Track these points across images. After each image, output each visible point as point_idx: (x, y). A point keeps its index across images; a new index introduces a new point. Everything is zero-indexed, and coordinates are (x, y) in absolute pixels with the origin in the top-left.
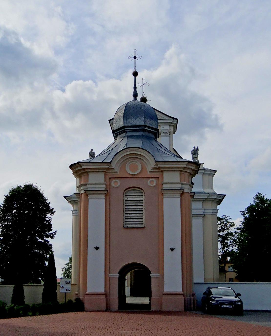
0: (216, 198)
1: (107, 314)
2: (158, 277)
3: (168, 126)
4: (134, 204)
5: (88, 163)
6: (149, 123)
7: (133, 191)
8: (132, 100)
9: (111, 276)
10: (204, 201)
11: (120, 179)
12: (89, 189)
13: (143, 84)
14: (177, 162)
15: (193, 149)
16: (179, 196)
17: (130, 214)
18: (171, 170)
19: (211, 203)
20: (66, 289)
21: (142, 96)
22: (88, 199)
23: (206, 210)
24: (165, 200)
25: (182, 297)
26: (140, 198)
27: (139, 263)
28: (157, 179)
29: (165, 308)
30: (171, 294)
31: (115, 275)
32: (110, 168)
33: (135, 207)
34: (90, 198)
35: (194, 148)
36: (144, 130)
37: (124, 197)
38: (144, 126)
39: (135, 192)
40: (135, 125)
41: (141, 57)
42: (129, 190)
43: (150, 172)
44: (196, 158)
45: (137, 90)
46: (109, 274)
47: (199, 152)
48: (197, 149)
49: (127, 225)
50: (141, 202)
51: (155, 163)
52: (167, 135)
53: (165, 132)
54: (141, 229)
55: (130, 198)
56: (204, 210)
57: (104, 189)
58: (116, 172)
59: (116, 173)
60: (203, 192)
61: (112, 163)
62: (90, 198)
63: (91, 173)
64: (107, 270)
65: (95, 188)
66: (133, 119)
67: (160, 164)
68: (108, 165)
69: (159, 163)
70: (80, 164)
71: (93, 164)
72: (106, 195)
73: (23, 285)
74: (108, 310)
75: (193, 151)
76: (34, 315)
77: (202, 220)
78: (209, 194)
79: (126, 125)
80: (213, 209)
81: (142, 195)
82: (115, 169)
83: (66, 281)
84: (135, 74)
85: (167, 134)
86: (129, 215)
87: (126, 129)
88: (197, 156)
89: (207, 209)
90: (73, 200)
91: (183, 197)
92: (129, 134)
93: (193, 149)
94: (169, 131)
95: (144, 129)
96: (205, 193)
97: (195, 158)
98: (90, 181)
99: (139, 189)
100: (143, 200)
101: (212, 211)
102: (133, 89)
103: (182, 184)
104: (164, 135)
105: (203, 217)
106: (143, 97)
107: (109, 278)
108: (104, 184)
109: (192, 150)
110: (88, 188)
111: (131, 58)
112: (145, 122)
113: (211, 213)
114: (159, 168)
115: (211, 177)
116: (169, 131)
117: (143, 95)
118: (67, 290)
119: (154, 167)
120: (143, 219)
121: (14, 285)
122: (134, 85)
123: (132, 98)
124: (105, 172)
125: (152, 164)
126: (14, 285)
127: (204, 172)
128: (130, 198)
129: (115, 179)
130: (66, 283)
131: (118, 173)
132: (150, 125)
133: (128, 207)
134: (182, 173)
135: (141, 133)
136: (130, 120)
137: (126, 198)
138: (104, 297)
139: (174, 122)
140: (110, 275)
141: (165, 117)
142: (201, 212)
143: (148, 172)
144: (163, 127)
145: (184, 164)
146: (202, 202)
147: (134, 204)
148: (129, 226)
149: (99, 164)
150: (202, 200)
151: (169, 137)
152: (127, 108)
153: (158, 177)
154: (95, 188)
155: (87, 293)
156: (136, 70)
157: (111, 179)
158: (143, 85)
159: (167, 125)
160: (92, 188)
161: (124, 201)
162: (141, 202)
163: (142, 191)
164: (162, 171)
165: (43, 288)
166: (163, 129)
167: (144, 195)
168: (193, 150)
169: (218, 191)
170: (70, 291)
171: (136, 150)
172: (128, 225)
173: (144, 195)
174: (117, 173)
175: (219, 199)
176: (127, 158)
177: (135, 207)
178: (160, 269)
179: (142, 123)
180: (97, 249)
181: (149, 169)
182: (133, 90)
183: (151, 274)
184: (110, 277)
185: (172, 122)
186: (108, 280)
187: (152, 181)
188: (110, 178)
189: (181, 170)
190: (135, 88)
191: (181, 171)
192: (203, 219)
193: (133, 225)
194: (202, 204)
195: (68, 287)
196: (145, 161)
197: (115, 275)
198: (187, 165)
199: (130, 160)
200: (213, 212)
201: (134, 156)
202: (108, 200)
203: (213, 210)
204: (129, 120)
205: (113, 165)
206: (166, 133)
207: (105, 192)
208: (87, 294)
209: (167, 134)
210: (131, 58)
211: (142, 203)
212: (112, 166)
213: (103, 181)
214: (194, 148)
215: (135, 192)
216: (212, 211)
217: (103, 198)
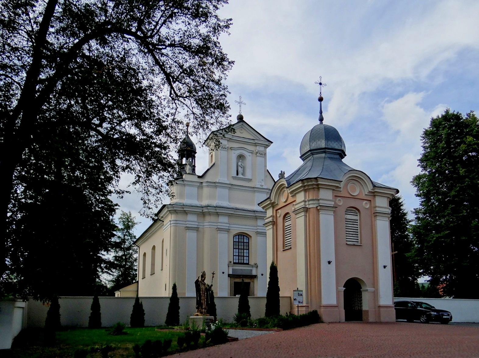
15: (280, 173)
21: (239, 114)
29: (383, 320)
30: (385, 307)
33: (352, 226)
35: (282, 171)
39: (352, 212)
43: (366, 195)
45: (323, 114)
51: (372, 187)
57: (332, 206)
63: (322, 189)
65: (327, 204)
73: (99, 297)
79: (327, 147)
81: (357, 215)
87: (327, 150)
90: (175, 209)
93: (280, 173)
98: (320, 197)
99: (355, 210)
104: (260, 155)
108: (332, 201)
111: (317, 83)
118: (299, 302)
119: (371, 191)
120: (358, 237)
121: (93, 297)
122: (319, 110)
123: (319, 123)
126: (93, 297)
135: (323, 155)
143: (364, 194)
151: (264, 158)
153: (370, 201)
154: (327, 204)
162: (357, 221)
163: (357, 212)
166: (259, 149)
167: (358, 216)
173: (358, 216)
177: (352, 226)
182: (319, 114)
187: (339, 200)
189: (389, 196)
193: (354, 243)
202: (182, 212)
210: (317, 83)
211: (357, 222)
215: (352, 212)
217: (332, 215)
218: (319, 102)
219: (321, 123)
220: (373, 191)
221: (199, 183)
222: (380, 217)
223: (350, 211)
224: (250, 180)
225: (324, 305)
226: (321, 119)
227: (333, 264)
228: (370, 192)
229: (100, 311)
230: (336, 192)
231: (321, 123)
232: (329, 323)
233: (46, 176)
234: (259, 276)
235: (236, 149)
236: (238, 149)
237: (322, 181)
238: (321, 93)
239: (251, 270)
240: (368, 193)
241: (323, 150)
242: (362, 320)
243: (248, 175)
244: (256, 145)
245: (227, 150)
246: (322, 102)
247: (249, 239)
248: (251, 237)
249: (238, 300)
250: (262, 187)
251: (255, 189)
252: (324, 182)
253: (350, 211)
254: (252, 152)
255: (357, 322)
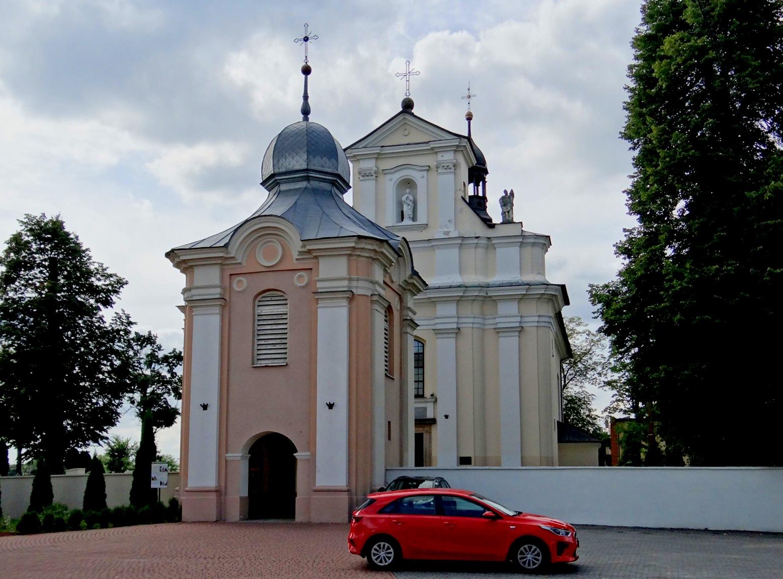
0: (543, 292)
1: (218, 529)
2: (307, 458)
3: (452, 153)
4: (272, 322)
5: (188, 250)
6: (319, 163)
7: (271, 298)
8: (296, 122)
9: (229, 457)
10: (522, 299)
11: (245, 276)
12: (194, 298)
13: (408, 73)
14: (337, 239)
15: (504, 195)
16: (345, 303)
17: (266, 341)
18: (332, 253)
19: (537, 302)
20: (161, 482)
21: (406, 97)
22: (193, 316)
23: (460, 324)
24: (320, 312)
25: (345, 496)
26: (282, 310)
27: (277, 433)
28: (310, 271)
30: (329, 491)
31: (235, 455)
32: (226, 256)
33: (274, 327)
34: (195, 313)
35: (505, 192)
36: (308, 179)
37: (256, 308)
38: (307, 170)
39: (274, 298)
40: (292, 169)
41: (296, 41)
42: (264, 295)
43: (297, 259)
44: (508, 212)
46: (226, 453)
47: (515, 201)
48: (510, 193)
49: (259, 362)
50: (284, 317)
52: (449, 170)
53: (446, 165)
54: (281, 368)
55: (266, 310)
56: (521, 317)
57: (218, 296)
58: (240, 263)
59: (239, 266)
60: (520, 282)
61: (230, 247)
62: (195, 315)
64: (223, 445)
65: (207, 295)
66: (289, 159)
67: (310, 245)
68: (222, 252)
69: (309, 242)
70: (175, 252)
71: (199, 251)
72: (223, 307)
74: (221, 520)
75: (503, 198)
76: (90, 527)
77: (454, 339)
78: (528, 284)
79: (277, 171)
80: (538, 314)
82: (237, 257)
83: (161, 467)
84: (307, 71)
85: (450, 168)
86: (263, 342)
88: (509, 209)
89: (526, 315)
91: (354, 304)
92: (283, 187)
93: (504, 195)
94: (452, 163)
95: (308, 176)
96: (518, 284)
97: (507, 213)
100: (287, 314)
101: (536, 319)
102: (302, 99)
103: (350, 280)
105: (457, 333)
106: (407, 98)
107: (226, 461)
109: (500, 197)
110: (193, 296)
111: (299, 40)
112: (308, 161)
113: (536, 324)
114: (309, 251)
115: (538, 250)
116: (452, 163)
117: (408, 94)
118: (161, 483)
119: (301, 250)
122: (303, 92)
124: (221, 264)
125: (296, 246)
127: (521, 240)
128: (266, 310)
129: (300, 271)
130: (160, 470)
131: (244, 264)
132: (319, 168)
133: (262, 328)
134: (353, 258)
135: (303, 184)
136: (292, 159)
137: (260, 311)
138: (213, 497)
139: (462, 143)
140: (226, 455)
141: (444, 136)
142: (514, 322)
144: (442, 156)
145: (350, 242)
146: (519, 303)
147: (272, 322)
148: (263, 363)
149: (206, 250)
150: (470, 298)
152: (281, 138)
153: (311, 269)
155: (187, 489)
156: (308, 63)
157: (233, 277)
158: (408, 76)
159: (450, 150)
160: (199, 295)
161: (256, 316)
162: (284, 317)
164: (316, 257)
165: (132, 479)
168: (503, 197)
169: (554, 278)
170: (166, 485)
171: (270, 220)
172: (263, 362)
174: (242, 266)
175: (551, 294)
176: (258, 235)
177: (274, 327)
178: (311, 444)
179: (304, 166)
180: (205, 407)
181: (295, 255)
182: (302, 101)
183: (296, 451)
184: (228, 459)
185: (458, 144)
186: (223, 466)
187: (301, 276)
188: (231, 275)
190: (306, 97)
191: (350, 255)
192: (519, 337)
194: (455, 308)
195: (163, 477)
196: (287, 238)
197: (235, 455)
198: (356, 243)
199: (260, 241)
200: (540, 322)
201: (271, 232)
202: (227, 316)
203: (539, 316)
204: (282, 161)
205: (233, 251)
206: (448, 166)
207: (222, 302)
208: (186, 491)
209: (450, 168)
210: (299, 40)
212: (230, 253)
213: (217, 281)
214: (505, 192)
215: (274, 298)
216: (536, 319)
217: (217, 314)
218: (304, 76)
219: (306, 119)
220: (304, 250)
221: (351, 249)
222: (324, 302)
223: (269, 299)
224: (426, 226)
225: (192, 489)
226: (306, 111)
227: (321, 401)
228: (301, 253)
229: (105, 491)
230: (231, 267)
231: (306, 119)
232: (192, 522)
233: (60, 293)
234: (440, 419)
235: (392, 171)
236: (397, 169)
237: (186, 255)
238: (306, 57)
239: (425, 409)
240: (298, 255)
241: (306, 174)
242: (181, 521)
243: (422, 219)
244: (434, 151)
245: (374, 177)
246: (309, 76)
247: (423, 347)
248: (425, 341)
249: (87, 480)
250: (448, 237)
251: (433, 244)
252: (190, 255)
253: (269, 299)
254: (428, 169)
255: (285, 521)
